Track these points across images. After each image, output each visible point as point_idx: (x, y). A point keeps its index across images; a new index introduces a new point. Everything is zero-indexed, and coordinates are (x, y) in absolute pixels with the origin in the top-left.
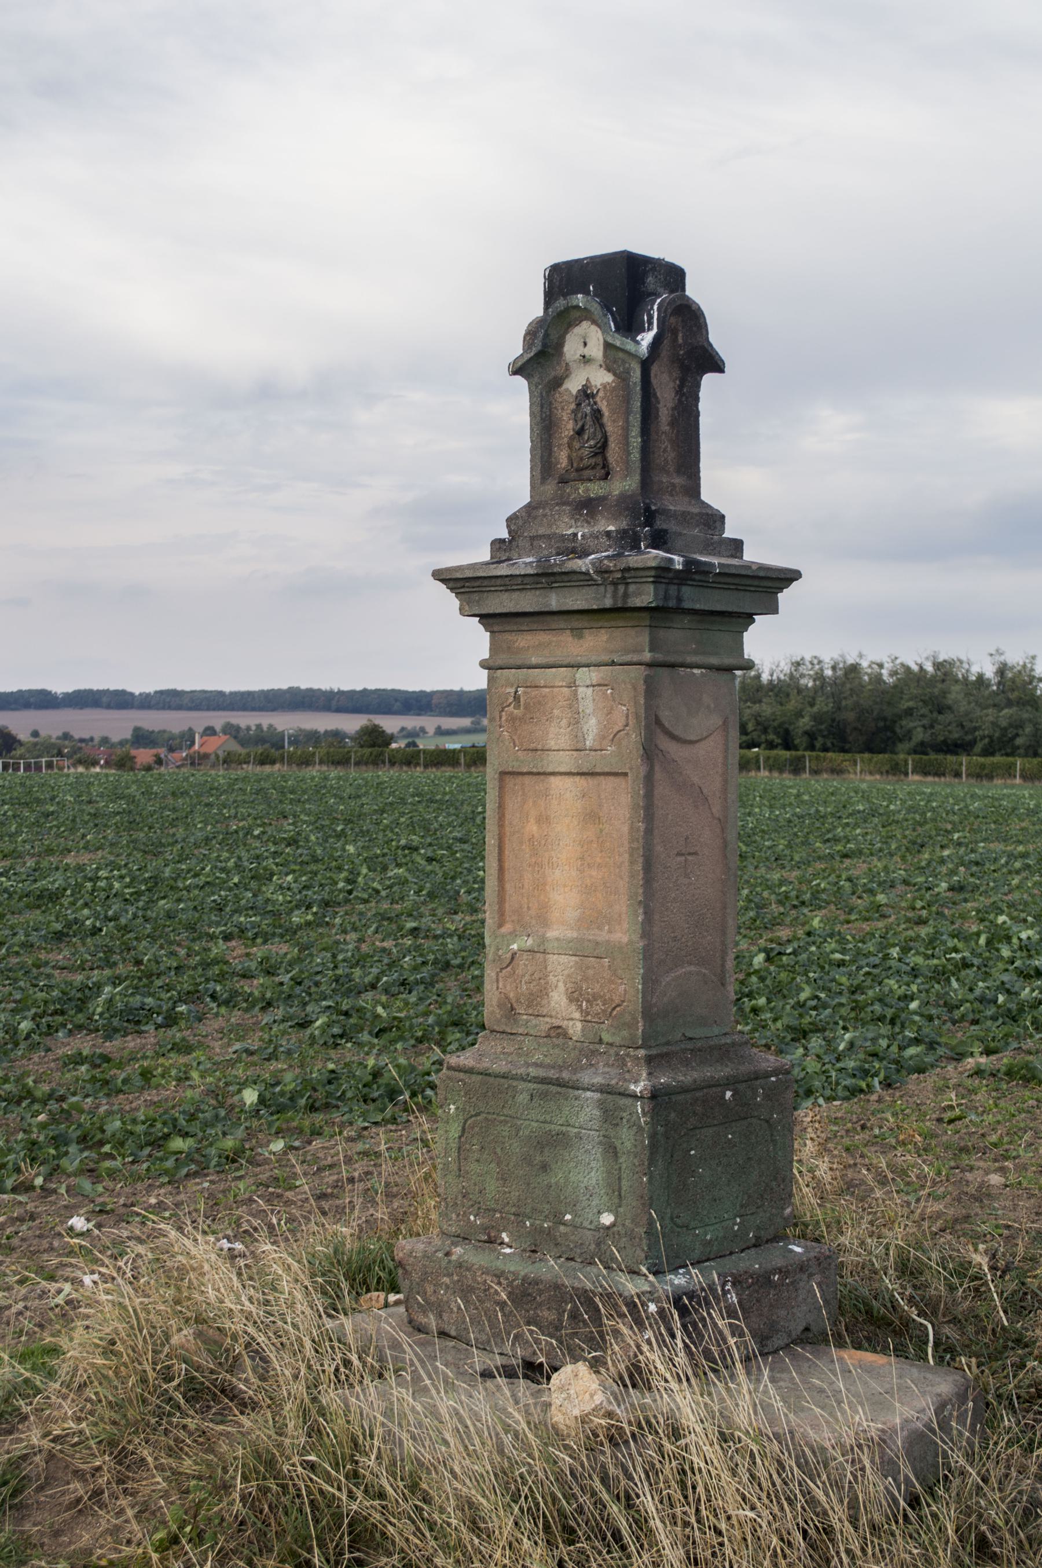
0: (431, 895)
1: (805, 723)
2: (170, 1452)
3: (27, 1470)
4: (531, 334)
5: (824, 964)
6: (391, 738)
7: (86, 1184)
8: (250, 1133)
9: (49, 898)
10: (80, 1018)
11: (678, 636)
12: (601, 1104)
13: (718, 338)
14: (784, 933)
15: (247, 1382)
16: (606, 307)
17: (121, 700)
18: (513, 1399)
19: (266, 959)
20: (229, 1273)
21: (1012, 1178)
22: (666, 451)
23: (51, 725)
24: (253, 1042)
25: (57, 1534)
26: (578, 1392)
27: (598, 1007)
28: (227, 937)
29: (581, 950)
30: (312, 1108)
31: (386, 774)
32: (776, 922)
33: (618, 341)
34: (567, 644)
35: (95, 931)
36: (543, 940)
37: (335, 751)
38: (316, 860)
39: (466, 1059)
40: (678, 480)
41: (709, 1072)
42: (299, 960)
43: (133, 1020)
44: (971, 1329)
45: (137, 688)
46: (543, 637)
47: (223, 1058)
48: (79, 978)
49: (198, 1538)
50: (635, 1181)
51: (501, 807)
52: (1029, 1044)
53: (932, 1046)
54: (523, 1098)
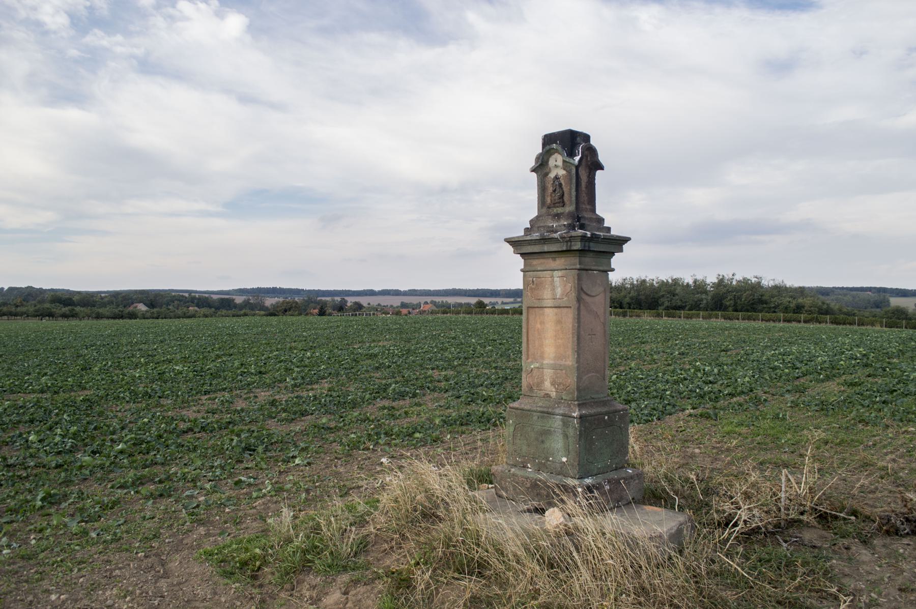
0: (501, 356)
1: (627, 300)
2: (416, 535)
3: (369, 539)
4: (537, 158)
5: (636, 379)
6: (487, 305)
7: (387, 448)
8: (441, 433)
9: (373, 356)
10: (384, 395)
11: (589, 260)
12: (562, 420)
13: (602, 158)
14: (622, 369)
15: (441, 513)
16: (563, 148)
17: (397, 293)
18: (530, 522)
19: (446, 375)
20: (434, 475)
21: (703, 450)
22: (584, 197)
23: (374, 301)
24: (442, 403)
25: (379, 560)
26: (554, 518)
27: (561, 387)
28: (433, 369)
29: (555, 367)
30: (462, 425)
31: (485, 316)
32: (619, 365)
33: (567, 159)
34: (550, 263)
35: (389, 367)
36: (542, 364)
37: (468, 310)
38: (462, 344)
39: (515, 405)
40: (588, 207)
41: (599, 410)
42: (456, 376)
43: (402, 395)
44: (690, 501)
45: (403, 288)
46: (542, 261)
47: (432, 407)
48: (384, 382)
49: (426, 563)
50: (574, 446)
51: (528, 319)
52: (708, 406)
53: (674, 406)
54: (535, 418)
